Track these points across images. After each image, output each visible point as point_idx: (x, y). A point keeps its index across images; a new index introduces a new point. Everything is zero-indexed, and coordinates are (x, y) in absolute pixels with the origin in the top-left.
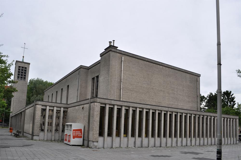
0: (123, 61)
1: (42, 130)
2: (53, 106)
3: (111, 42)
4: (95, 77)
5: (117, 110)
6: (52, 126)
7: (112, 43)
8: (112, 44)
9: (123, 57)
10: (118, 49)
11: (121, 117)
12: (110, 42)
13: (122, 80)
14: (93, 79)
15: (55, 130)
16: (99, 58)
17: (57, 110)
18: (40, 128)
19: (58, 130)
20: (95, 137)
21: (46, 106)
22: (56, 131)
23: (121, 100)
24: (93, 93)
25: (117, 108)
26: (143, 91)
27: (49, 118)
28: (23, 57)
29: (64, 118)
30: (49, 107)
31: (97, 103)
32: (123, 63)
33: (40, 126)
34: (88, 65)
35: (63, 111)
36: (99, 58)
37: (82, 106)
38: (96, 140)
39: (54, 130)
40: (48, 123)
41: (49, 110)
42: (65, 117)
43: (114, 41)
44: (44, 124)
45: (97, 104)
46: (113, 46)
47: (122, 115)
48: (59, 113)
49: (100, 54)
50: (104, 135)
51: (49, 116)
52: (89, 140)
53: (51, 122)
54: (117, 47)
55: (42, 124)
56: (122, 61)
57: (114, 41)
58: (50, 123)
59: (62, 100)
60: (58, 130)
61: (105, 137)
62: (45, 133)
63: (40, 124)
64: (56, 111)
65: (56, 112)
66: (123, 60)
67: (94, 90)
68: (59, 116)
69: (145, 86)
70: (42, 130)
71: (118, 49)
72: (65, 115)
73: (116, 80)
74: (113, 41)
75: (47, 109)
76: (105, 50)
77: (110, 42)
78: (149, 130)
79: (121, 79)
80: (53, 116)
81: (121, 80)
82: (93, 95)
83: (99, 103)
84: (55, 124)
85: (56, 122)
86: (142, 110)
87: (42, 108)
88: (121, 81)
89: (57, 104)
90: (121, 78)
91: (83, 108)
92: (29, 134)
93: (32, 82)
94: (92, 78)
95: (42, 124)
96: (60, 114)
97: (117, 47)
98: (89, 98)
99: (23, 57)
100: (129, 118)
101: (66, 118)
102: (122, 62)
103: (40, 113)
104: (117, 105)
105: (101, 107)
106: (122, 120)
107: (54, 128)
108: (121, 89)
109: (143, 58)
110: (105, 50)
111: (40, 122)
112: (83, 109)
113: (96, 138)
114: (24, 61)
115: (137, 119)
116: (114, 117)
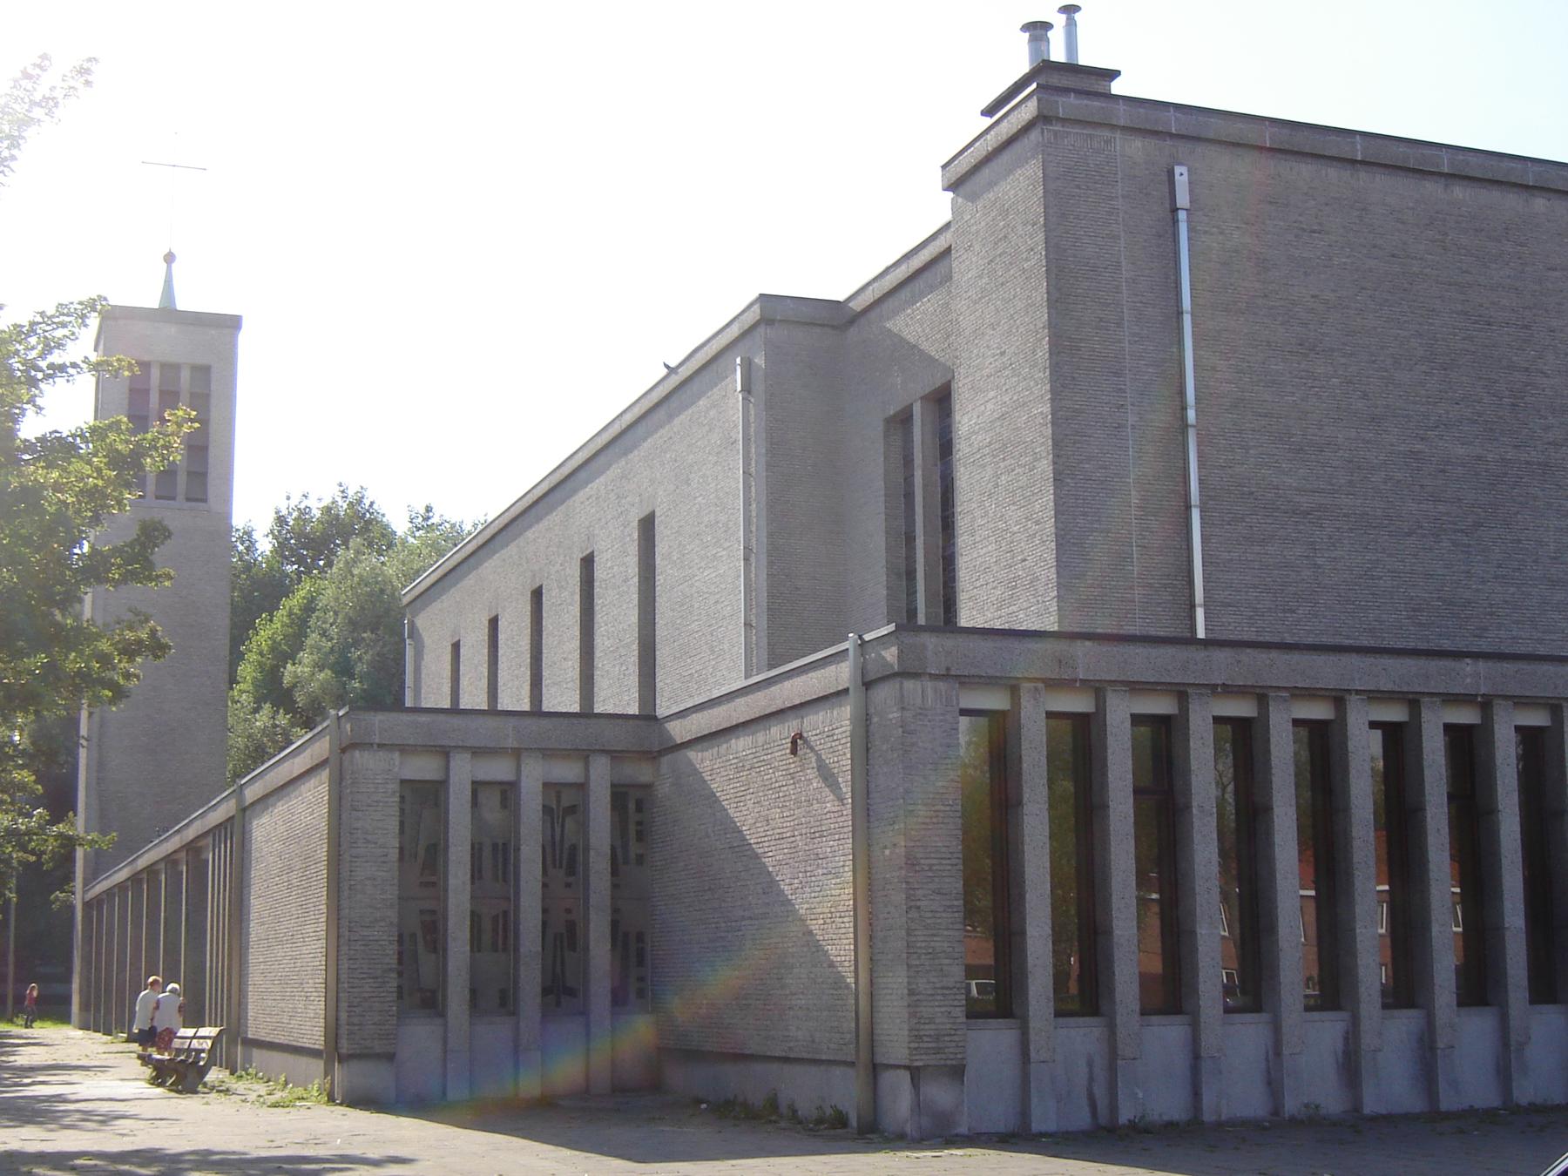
0: (1182, 215)
1: (430, 1002)
2: (511, 743)
3: (1047, 26)
4: (917, 409)
5: (1134, 739)
6: (517, 950)
7: (1050, 34)
8: (1058, 54)
9: (1178, 170)
10: (1117, 87)
11: (1188, 807)
12: (1037, 30)
13: (1191, 415)
14: (903, 420)
15: (546, 991)
16: (937, 208)
17: (545, 785)
18: (400, 974)
19: (571, 992)
20: (931, 1021)
21: (445, 753)
22: (558, 1004)
23: (1201, 634)
24: (911, 574)
25: (1137, 719)
26: (1441, 508)
27: (476, 874)
28: (170, 258)
29: (626, 862)
30: (468, 756)
31: (929, 685)
32: (1190, 230)
33: (400, 961)
34: (836, 288)
35: (613, 785)
36: (937, 208)
37: (788, 728)
38: (938, 1051)
39: (539, 990)
40: (475, 918)
41: (477, 786)
42: (634, 849)
43: (1077, 16)
44: (432, 930)
45: (930, 692)
46: (1072, 69)
47: (1188, 784)
48: (572, 810)
49: (944, 167)
50: (1025, 1003)
51: (476, 851)
52: (880, 1059)
53: (505, 913)
54: (1114, 74)
55: (413, 935)
56: (1175, 210)
57: (1069, 10)
58: (495, 919)
59: (597, 673)
60: (571, 992)
61: (1034, 1025)
62: (445, 1025)
63: (400, 936)
64: (539, 800)
65: (547, 810)
66: (1183, 199)
67: (910, 539)
68: (574, 848)
69: (1461, 451)
70: (430, 1002)
71: (1117, 87)
72: (632, 828)
73: (1132, 419)
74: (1063, 17)
75: (454, 779)
76: (988, 112)
77: (1037, 30)
78: (1499, 929)
79: (1184, 408)
80: (518, 850)
81: (1184, 418)
82: (911, 592)
83: (942, 685)
84: (544, 924)
85: (545, 911)
86: (1548, 723)
87: (403, 782)
88: (1185, 426)
89: (545, 722)
90: (1182, 392)
91: (796, 743)
92: (1113, 127)
93: (299, 534)
94: (889, 421)
95: (419, 934)
96: (584, 827)
97: (1114, 74)
98: (469, 787)
99: (170, 258)
100: (1268, 809)
101: (640, 859)
102: (1175, 222)
103: (393, 824)
104: (1123, 683)
105: (1053, 722)
106: (1197, 837)
107: (531, 977)
108: (1188, 508)
109: (1402, 149)
110: (988, 121)
111: (392, 915)
112: (794, 752)
113: (937, 1038)
114: (179, 307)
115: (1354, 811)
116: (1105, 807)
